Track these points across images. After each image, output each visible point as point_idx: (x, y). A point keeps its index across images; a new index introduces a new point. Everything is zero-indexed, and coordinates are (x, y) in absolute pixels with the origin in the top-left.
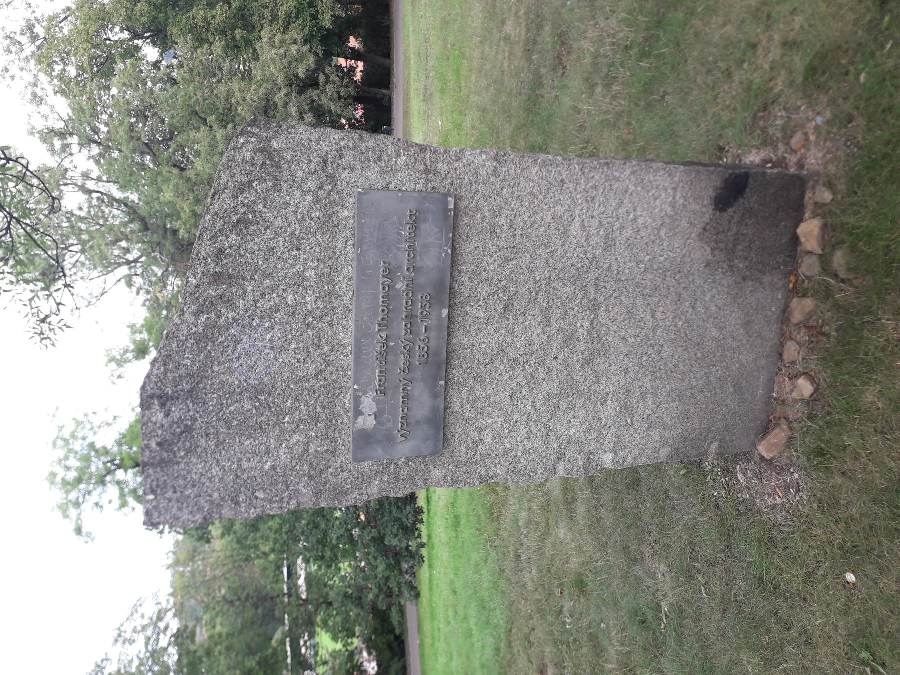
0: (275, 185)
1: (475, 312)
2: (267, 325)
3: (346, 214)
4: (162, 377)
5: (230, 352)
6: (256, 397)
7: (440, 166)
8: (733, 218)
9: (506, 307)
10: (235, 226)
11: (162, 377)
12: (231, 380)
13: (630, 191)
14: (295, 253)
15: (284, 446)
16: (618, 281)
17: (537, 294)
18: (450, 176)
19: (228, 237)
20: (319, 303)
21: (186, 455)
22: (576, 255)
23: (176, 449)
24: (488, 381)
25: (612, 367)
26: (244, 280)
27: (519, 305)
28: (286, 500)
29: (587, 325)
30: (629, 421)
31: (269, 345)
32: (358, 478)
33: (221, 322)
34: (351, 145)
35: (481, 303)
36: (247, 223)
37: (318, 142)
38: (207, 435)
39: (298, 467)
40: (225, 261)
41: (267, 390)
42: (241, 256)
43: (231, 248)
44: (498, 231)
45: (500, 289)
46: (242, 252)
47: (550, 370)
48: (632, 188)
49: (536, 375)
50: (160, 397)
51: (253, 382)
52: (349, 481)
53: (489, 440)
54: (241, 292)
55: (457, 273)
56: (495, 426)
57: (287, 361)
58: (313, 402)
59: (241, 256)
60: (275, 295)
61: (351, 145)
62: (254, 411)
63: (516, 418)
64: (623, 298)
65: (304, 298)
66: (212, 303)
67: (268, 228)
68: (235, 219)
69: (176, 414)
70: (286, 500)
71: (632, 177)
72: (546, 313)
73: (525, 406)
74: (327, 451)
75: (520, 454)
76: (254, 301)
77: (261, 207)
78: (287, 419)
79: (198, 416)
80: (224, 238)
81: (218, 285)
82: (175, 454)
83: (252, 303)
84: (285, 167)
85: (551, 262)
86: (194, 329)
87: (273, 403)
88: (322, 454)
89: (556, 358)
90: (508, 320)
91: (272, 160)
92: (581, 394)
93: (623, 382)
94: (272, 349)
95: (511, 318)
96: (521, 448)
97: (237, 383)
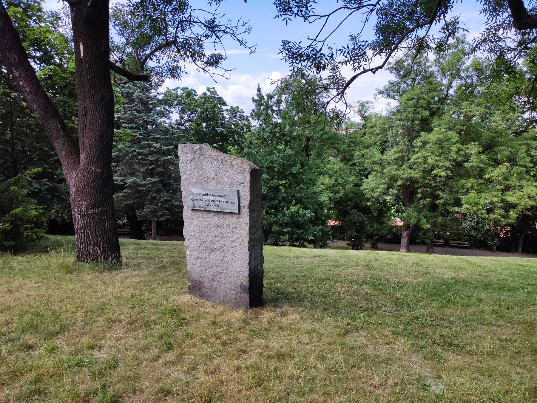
27: (219, 229)
69: (198, 151)
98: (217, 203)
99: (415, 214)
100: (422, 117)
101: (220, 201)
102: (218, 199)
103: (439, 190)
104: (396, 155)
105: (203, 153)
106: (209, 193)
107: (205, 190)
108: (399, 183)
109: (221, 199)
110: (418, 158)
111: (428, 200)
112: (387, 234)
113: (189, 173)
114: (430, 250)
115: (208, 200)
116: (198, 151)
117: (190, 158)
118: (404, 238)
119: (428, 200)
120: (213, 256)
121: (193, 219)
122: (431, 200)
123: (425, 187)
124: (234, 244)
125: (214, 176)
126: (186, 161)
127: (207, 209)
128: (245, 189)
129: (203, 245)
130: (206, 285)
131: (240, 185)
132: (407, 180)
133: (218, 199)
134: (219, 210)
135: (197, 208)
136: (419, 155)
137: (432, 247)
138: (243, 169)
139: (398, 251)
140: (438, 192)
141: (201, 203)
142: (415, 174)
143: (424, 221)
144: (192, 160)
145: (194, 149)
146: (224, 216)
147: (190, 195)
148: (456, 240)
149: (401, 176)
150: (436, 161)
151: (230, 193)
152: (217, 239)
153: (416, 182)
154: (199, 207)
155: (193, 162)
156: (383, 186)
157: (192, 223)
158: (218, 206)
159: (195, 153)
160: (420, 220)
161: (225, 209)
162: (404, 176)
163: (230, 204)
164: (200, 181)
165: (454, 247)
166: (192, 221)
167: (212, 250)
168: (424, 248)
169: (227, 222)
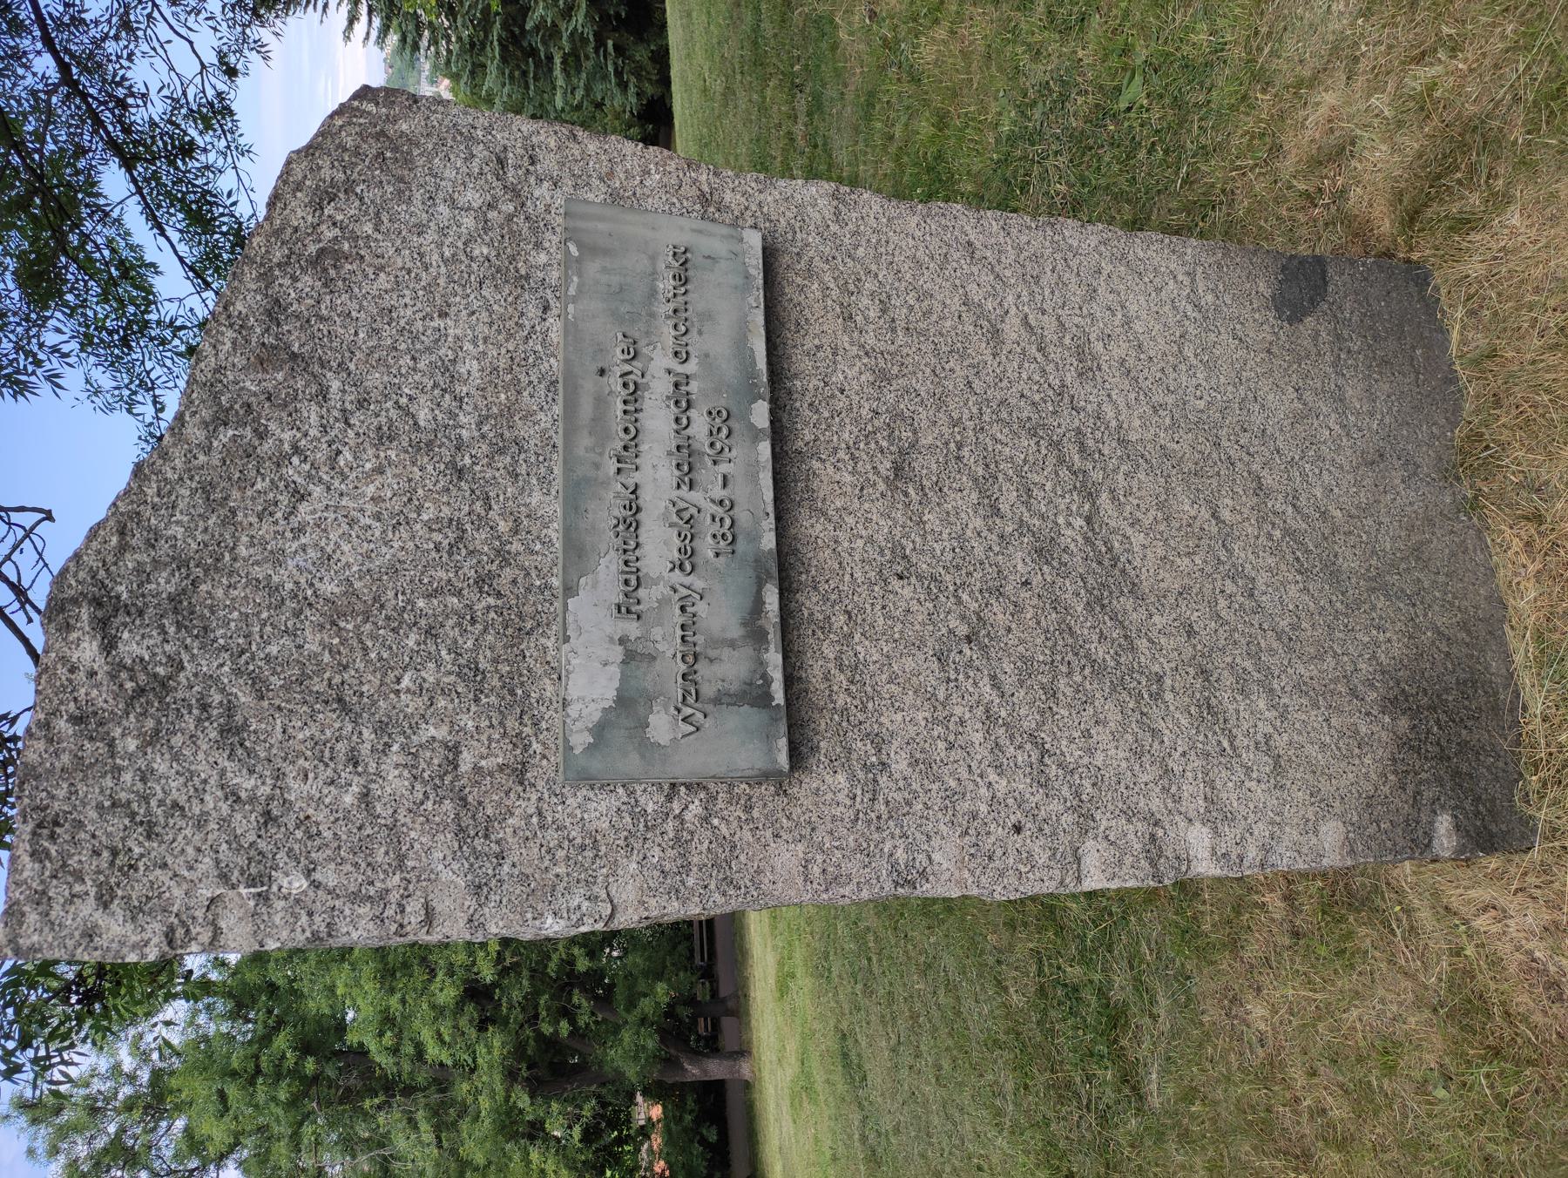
0: (400, 192)
1: (831, 470)
2: (368, 466)
3: (543, 258)
4: (110, 559)
5: (279, 515)
6: (334, 623)
7: (728, 196)
8: (1317, 333)
9: (897, 469)
10: (316, 261)
11: (110, 559)
12: (276, 579)
13: (1105, 273)
14: (437, 322)
15: (395, 748)
16: (1121, 442)
17: (959, 446)
18: (749, 213)
19: (295, 279)
20: (485, 428)
21: (142, 748)
22: (1024, 376)
23: (117, 732)
24: (881, 621)
25: (1156, 619)
26: (323, 367)
27: (926, 465)
28: (394, 897)
29: (1079, 522)
30: (1226, 744)
31: (370, 508)
32: (583, 848)
33: (267, 447)
34: (552, 144)
35: (841, 454)
36: (339, 257)
37: (488, 130)
38: (205, 707)
39: (429, 805)
40: (286, 328)
41: (359, 607)
42: (322, 319)
43: (299, 300)
44: (859, 319)
45: (878, 429)
46: (324, 312)
47: (1018, 608)
48: (1107, 268)
49: (986, 614)
50: (97, 602)
51: (329, 588)
52: (561, 854)
53: (903, 765)
54: (314, 388)
55: (783, 394)
56: (912, 730)
57: (410, 545)
58: (470, 644)
59: (322, 319)
60: (389, 404)
61: (552, 144)
62: (327, 658)
63: (958, 711)
64: (1142, 476)
65: (452, 415)
66: (248, 406)
67: (381, 269)
68: (313, 249)
69: (131, 646)
70: (394, 897)
71: (1102, 248)
72: (985, 486)
73: (975, 684)
74: (501, 768)
75: (984, 808)
76: (344, 411)
77: (368, 228)
78: (406, 682)
79: (185, 657)
80: (287, 282)
81: (265, 371)
82: (111, 744)
83: (336, 413)
84: (421, 162)
85: (977, 384)
86: (202, 458)
87: (374, 637)
88: (491, 774)
89: (1026, 583)
90: (906, 494)
91: (395, 149)
92: (1098, 670)
93: (1188, 652)
94: (378, 517)
95: (911, 491)
96: (983, 791)
97: (289, 586)
98: (700, 426)
99: (627, 1036)
100: (295, 1049)
101: (682, 401)
102: (658, 420)
103: (546, 966)
104: (424, 1126)
105: (165, 583)
106: (605, 511)
107: (576, 552)
108: (523, 1100)
109: (659, 387)
110: (439, 1035)
111: (577, 998)
112: (703, 1141)
113: (395, 781)
114: (730, 1004)
115: (687, 523)
116: (131, 646)
117: (206, 760)
118: (705, 1072)
119: (577, 998)
120: (1142, 551)
121: (878, 741)
122: (576, 991)
123: (536, 1016)
124: (1012, 330)
125: (429, 473)
126: (245, 824)
127: (769, 541)
128: (548, 163)
129: (1100, 651)
130: (1394, 647)
131: (515, 192)
132: (511, 1076)
133: (658, 420)
134: (760, 414)
135: (774, 658)
136: (426, 1036)
137: (723, 1001)
138: (371, 148)
139: (747, 1086)
140: (552, 966)
141: (720, 615)
142: (493, 1048)
143: (646, 1005)
144: (232, 733)
145: (102, 698)
146: (802, 405)
147: (647, 747)
148: (692, 951)
149: (500, 1098)
150: (451, 973)
151: (593, 267)
152: (1008, 498)
153: (519, 1051)
154: (757, 636)
155: (269, 731)
156: (535, 1155)
157: (923, 764)
158: (724, 420)
159: (150, 691)
160: (643, 1021)
161: (741, 342)
162: (499, 1087)
163: (699, 300)
164: (488, 649)
165: (712, 954)
166: (900, 765)
167: (1111, 579)
168: (727, 1023)
169: (852, 374)
